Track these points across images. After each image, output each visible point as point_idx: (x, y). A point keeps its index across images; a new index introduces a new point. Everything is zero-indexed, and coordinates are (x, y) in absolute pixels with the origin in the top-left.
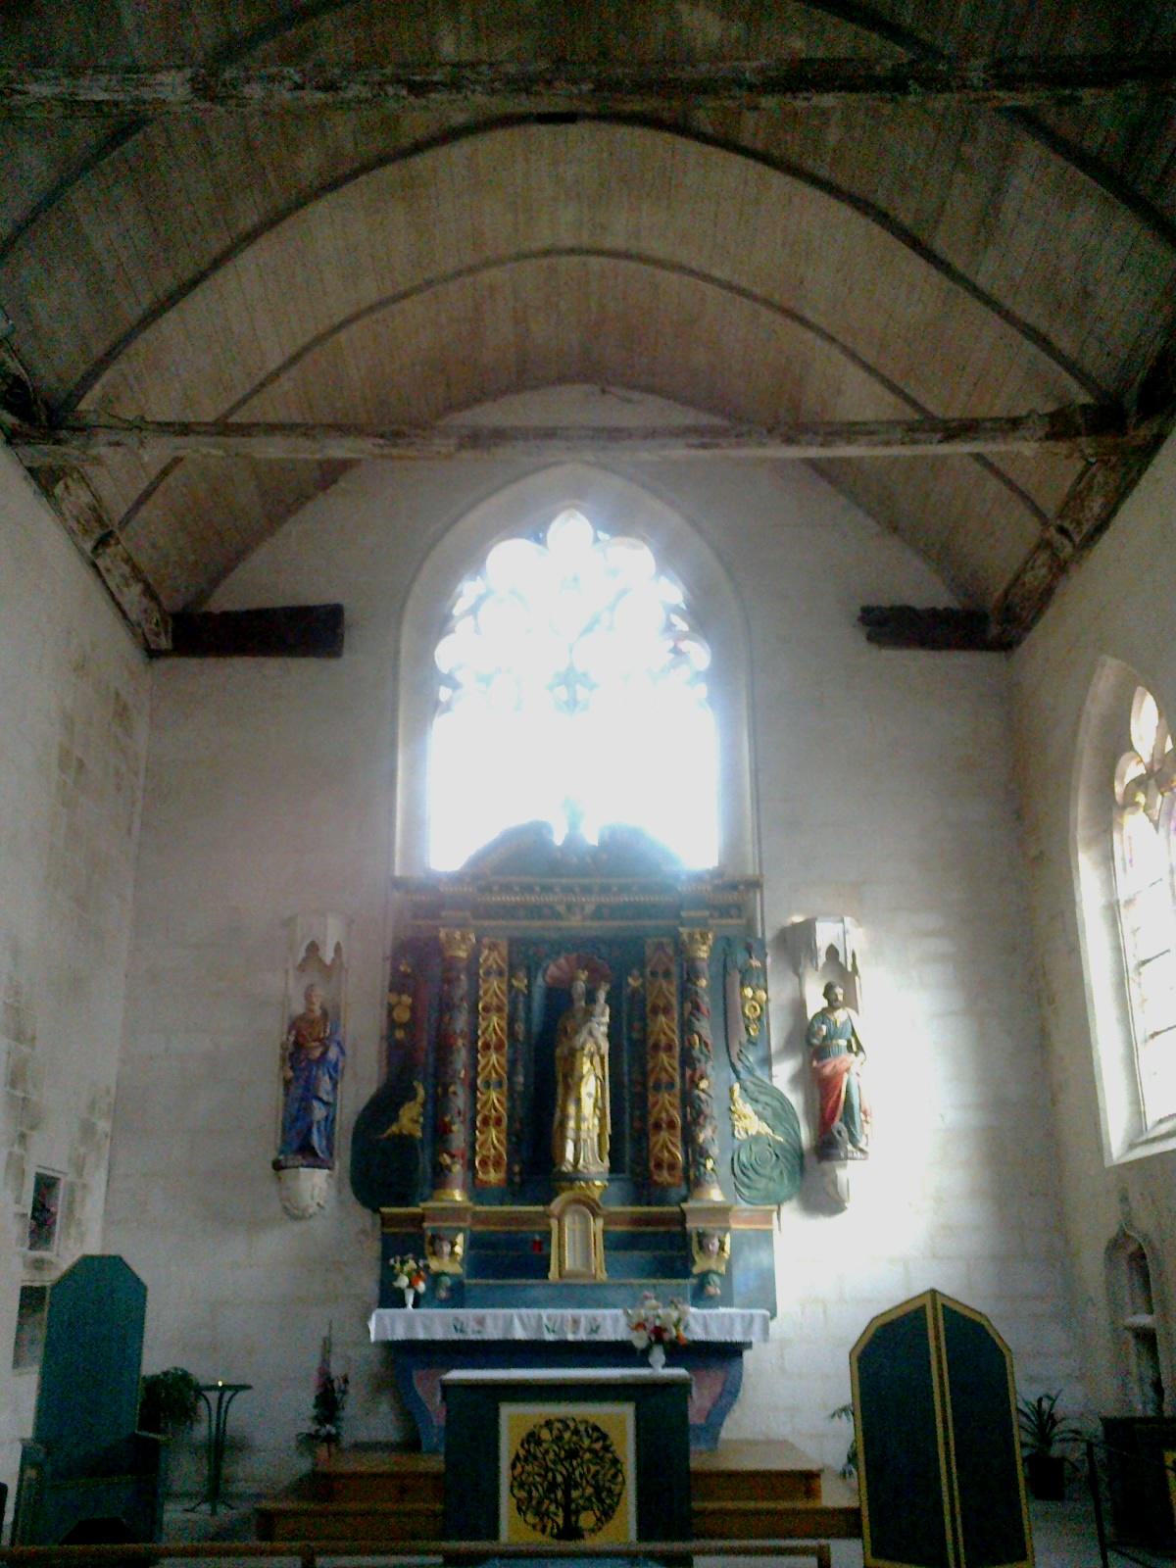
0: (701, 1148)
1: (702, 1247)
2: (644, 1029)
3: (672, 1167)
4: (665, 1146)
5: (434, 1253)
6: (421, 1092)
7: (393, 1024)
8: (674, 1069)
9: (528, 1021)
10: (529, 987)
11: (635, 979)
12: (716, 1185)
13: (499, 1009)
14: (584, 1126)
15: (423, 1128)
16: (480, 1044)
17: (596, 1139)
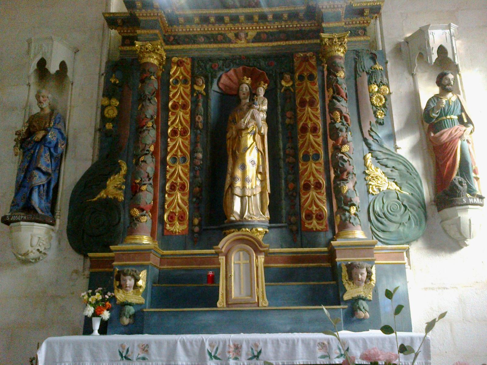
0: (345, 197)
1: (351, 278)
2: (295, 116)
3: (320, 217)
4: (313, 202)
5: (120, 287)
6: (124, 167)
7: (104, 119)
8: (319, 145)
9: (206, 115)
10: (206, 90)
11: (287, 82)
12: (360, 227)
13: (184, 107)
14: (248, 185)
15: (125, 193)
16: (169, 131)
17: (258, 196)
